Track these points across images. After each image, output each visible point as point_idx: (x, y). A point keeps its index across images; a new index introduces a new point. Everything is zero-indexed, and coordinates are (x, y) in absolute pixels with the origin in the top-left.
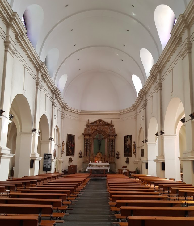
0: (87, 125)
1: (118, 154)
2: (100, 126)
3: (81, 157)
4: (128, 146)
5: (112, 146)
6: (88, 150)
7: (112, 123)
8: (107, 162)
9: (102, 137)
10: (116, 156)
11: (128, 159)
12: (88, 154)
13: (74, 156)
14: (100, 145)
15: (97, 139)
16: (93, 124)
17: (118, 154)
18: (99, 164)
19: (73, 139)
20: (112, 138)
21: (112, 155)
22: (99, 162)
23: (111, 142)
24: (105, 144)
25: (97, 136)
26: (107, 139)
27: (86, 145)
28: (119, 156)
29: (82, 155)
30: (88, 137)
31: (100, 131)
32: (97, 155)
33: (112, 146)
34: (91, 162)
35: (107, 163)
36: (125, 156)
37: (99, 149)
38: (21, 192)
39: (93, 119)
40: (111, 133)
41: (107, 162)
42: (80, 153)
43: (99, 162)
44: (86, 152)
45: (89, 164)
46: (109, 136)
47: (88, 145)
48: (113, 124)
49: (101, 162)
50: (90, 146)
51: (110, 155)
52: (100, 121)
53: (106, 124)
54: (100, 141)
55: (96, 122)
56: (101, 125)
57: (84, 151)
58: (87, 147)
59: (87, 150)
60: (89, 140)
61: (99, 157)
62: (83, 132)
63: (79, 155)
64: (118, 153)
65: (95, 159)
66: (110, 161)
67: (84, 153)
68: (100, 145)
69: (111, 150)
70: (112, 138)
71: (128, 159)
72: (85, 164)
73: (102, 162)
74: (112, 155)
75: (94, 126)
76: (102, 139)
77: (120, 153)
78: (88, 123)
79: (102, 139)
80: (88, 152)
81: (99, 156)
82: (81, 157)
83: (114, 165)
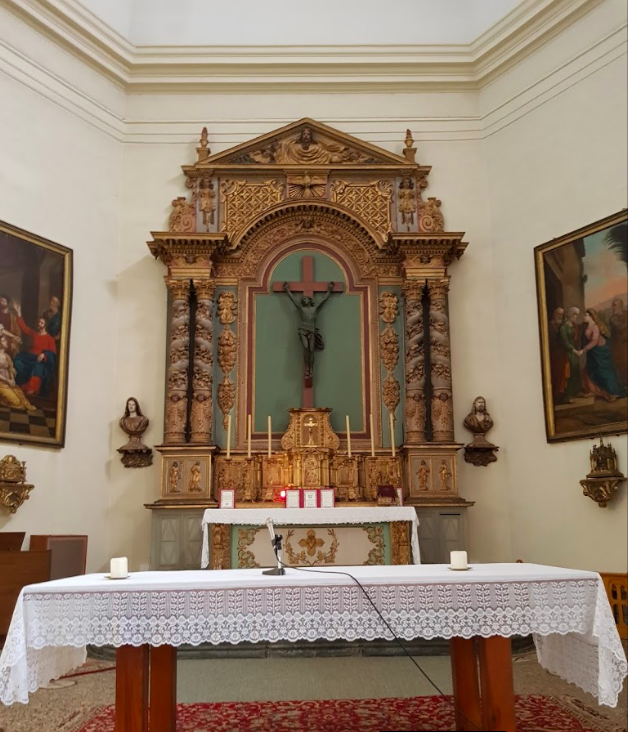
0: (192, 175)
1: (480, 418)
2: (312, 174)
3: (136, 457)
4: (594, 329)
5: (426, 344)
6: (202, 388)
7: (410, 152)
8: (394, 495)
9: (332, 269)
10: (464, 438)
11: (604, 458)
12: (201, 426)
13: (60, 445)
14: (311, 345)
15: (284, 290)
16: (240, 154)
17: (480, 418)
18: (310, 515)
19: (44, 284)
20: (419, 272)
21: (428, 432)
22: (310, 497)
23: (416, 314)
24: (357, 333)
25: (286, 269)
26: (378, 289)
27: (182, 340)
28: (493, 438)
29: (152, 439)
30: (200, 272)
31: (305, 216)
32: (287, 440)
33: (426, 344)
34: (227, 497)
35: (394, 503)
36: (561, 430)
37: (309, 383)
38: (363, 544)
39: (242, 121)
40: (419, 226)
41: (386, 493)
42: (133, 422)
43: (310, 497)
44: (182, 405)
45: (211, 516)
46: (396, 252)
47: (204, 343)
48: (422, 159)
49: (328, 496)
50: (220, 358)
51: (414, 425)
52: (307, 132)
53: (362, 162)
54: (309, 311)
55: (268, 144)
56: (319, 173)
57: (170, 399)
58: (192, 365)
59: (190, 392)
60: (205, 299)
61: (309, 453)
62: (161, 224)
63: (123, 441)
64: (483, 411)
65: (272, 475)
66: (415, 483)
67: (167, 415)
68: (311, 345)
69: (416, 385)
70: (419, 272)
71: (604, 458)
72: (170, 525)
73: (337, 500)
74: (428, 432)
75: (253, 185)
76: (333, 290)
77: (496, 413)
78: (204, 152)
79: (333, 290)
80: (201, 410)
81: (311, 445)
82: (136, 457)
83: (455, 521)
